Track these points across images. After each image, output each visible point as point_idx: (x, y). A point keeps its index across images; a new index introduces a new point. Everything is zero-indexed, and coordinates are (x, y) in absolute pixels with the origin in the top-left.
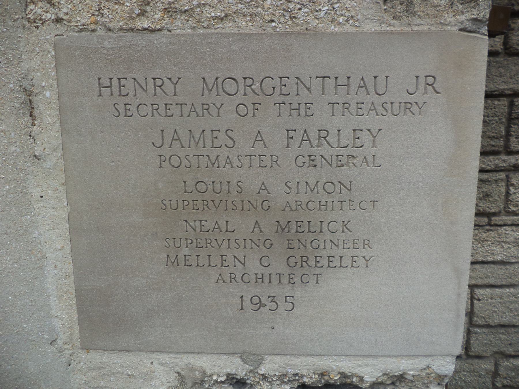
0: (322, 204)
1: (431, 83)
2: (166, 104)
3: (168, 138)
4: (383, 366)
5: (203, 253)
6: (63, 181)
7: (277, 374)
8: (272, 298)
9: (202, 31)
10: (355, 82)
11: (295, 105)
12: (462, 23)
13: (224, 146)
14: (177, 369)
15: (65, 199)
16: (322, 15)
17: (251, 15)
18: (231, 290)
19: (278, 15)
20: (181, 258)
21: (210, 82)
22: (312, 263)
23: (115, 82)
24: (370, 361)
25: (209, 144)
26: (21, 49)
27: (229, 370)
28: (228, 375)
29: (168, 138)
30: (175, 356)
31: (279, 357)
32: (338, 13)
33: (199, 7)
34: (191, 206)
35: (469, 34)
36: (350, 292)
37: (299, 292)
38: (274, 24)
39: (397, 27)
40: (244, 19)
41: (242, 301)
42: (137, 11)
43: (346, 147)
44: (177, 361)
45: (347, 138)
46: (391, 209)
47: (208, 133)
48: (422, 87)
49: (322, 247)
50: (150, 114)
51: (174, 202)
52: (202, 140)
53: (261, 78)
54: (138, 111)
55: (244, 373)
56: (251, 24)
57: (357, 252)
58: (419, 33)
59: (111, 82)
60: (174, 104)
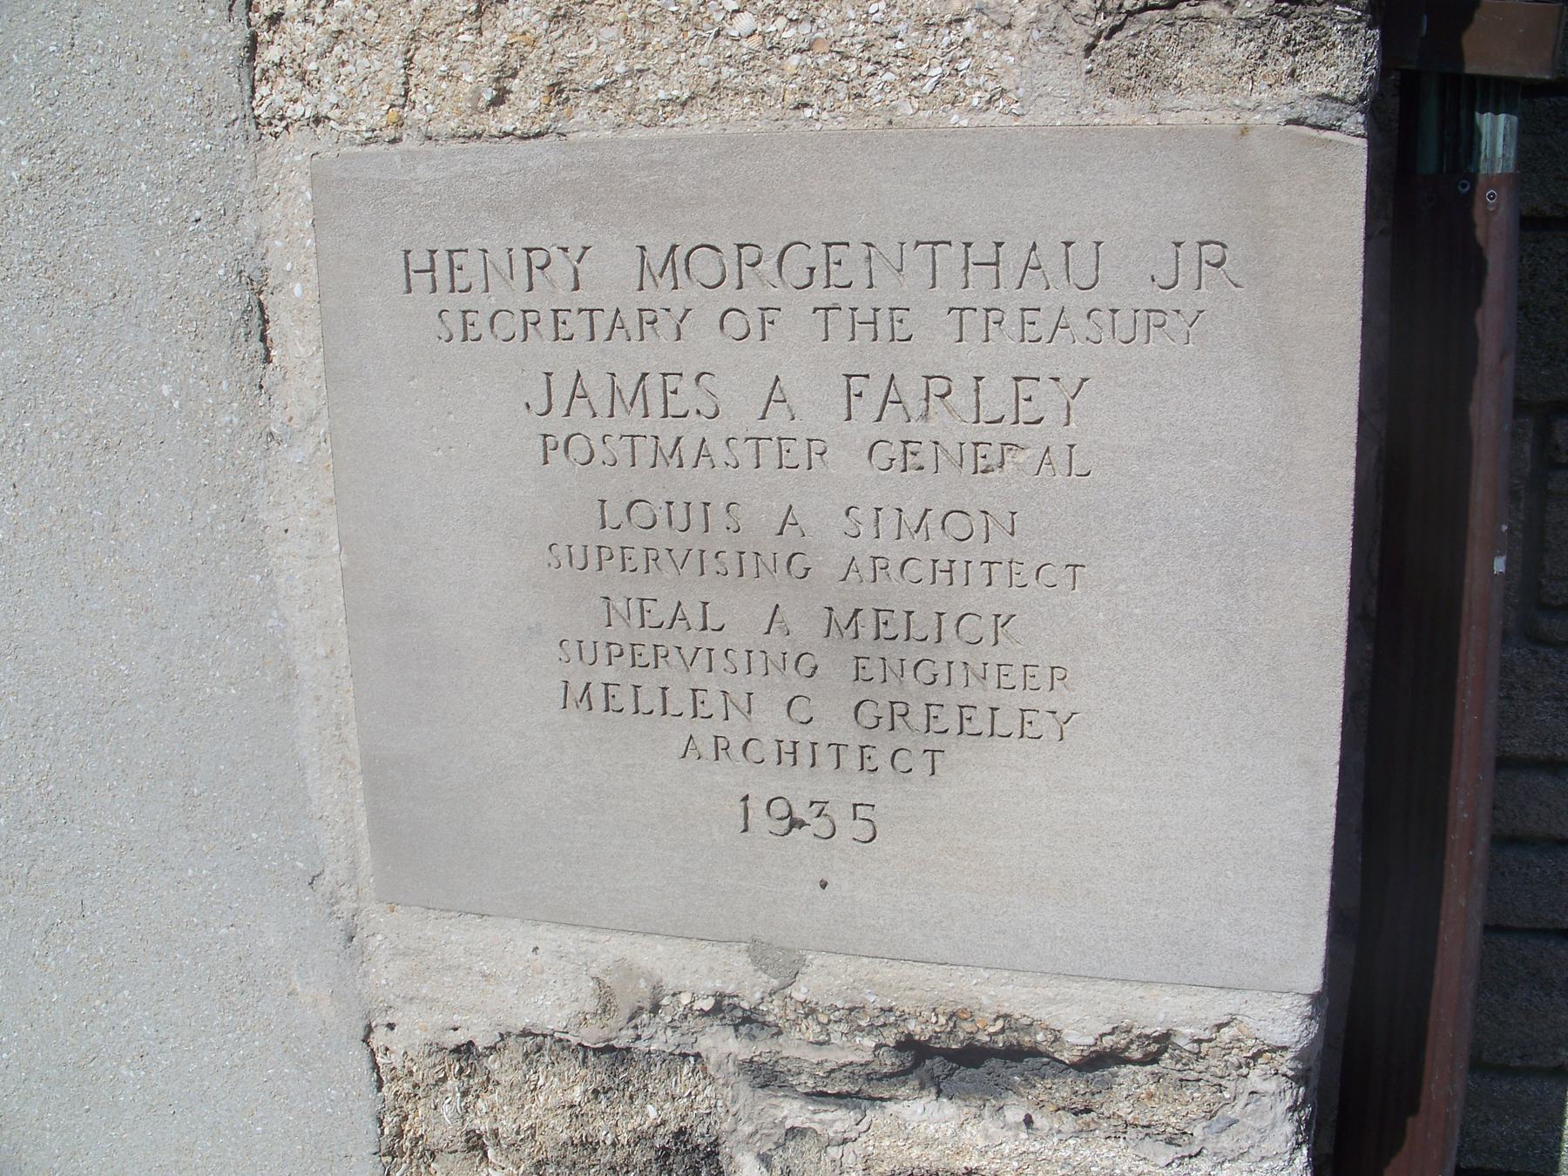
0: (975, 254)
1: (1214, 255)
2: (556, 311)
3: (561, 396)
4: (1114, 1006)
5: (650, 681)
6: (331, 494)
7: (839, 1004)
8: (820, 806)
9: (635, 134)
10: (1013, 258)
11: (865, 314)
12: (1291, 105)
13: (692, 413)
14: (595, 971)
15: (334, 538)
16: (927, 89)
17: (754, 92)
18: (718, 778)
19: (818, 90)
20: (597, 693)
21: (656, 258)
22: (917, 719)
23: (441, 260)
24: (1076, 988)
25: (656, 408)
26: (242, 188)
27: (718, 984)
28: (719, 997)
29: (561, 396)
30: (590, 936)
31: (841, 959)
32: (967, 81)
33: (630, 77)
34: (617, 561)
35: (1314, 132)
36: (1018, 804)
37: (886, 794)
38: (808, 112)
39: (1120, 111)
40: (738, 100)
41: (746, 809)
42: (488, 95)
43: (1000, 421)
44: (593, 948)
45: (997, 399)
46: (1122, 588)
47: (654, 381)
48: (1188, 271)
49: (943, 679)
50: (520, 334)
51: (577, 551)
52: (640, 396)
53: (781, 247)
54: (492, 326)
55: (758, 995)
56: (753, 113)
57: (1031, 700)
58: (1178, 131)
59: (432, 260)
60: (575, 310)
